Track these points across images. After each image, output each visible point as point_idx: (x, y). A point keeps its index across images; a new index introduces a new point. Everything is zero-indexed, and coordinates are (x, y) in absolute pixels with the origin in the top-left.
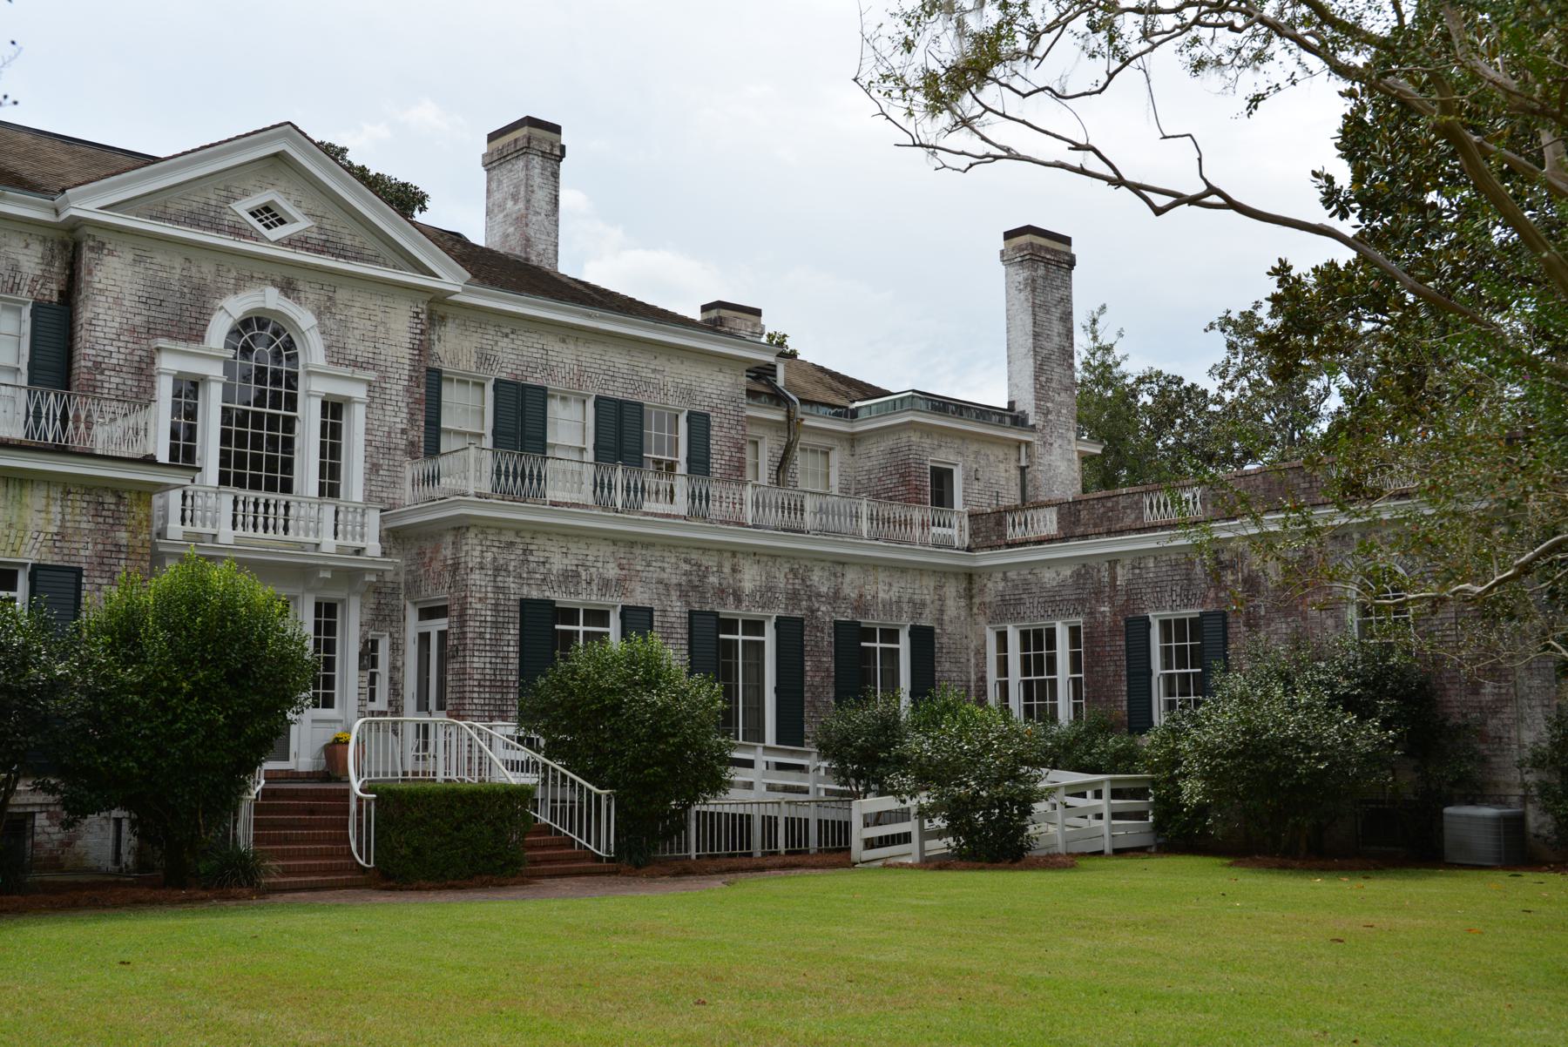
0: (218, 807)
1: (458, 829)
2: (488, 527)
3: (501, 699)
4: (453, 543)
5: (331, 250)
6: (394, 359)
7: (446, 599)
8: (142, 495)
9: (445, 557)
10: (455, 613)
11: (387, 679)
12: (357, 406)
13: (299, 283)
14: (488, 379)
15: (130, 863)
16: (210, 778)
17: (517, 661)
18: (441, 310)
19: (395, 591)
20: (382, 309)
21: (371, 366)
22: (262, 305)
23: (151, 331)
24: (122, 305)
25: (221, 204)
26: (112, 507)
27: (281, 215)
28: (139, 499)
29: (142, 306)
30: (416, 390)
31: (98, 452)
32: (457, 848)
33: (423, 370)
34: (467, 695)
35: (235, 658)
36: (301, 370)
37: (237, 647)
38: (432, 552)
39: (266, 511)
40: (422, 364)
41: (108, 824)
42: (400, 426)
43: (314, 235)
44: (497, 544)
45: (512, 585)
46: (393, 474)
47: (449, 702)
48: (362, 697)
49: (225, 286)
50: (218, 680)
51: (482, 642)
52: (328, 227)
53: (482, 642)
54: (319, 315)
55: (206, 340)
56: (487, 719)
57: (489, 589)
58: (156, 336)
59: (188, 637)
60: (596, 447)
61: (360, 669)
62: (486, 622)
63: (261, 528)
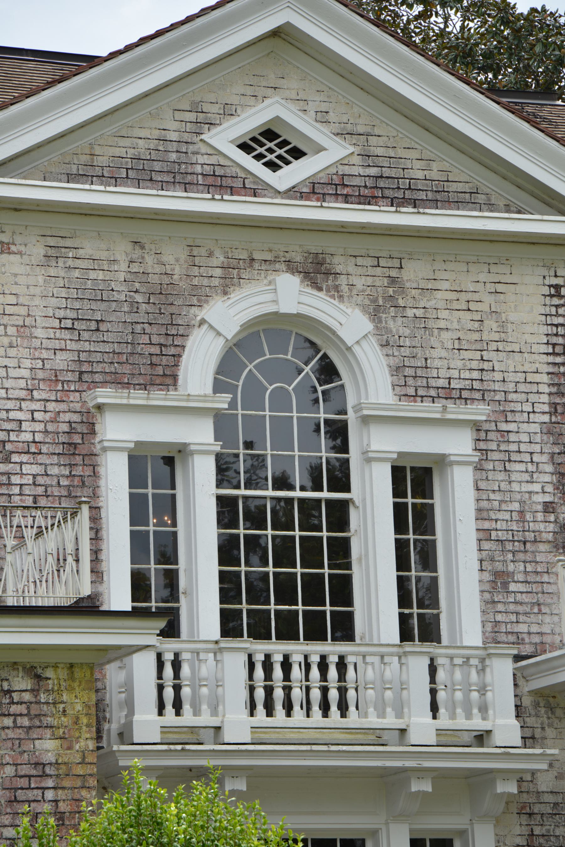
5: (387, 193)
6: (520, 377)
8: (76, 670)
13: (336, 260)
20: (491, 288)
21: (478, 395)
22: (272, 308)
23: (86, 377)
24: (32, 337)
25: (186, 137)
26: (27, 697)
27: (295, 142)
29: (66, 335)
31: (10, 602)
36: (351, 417)
39: (287, 677)
42: (540, 498)
43: (355, 171)
49: (205, 282)
52: (380, 151)
55: (180, 382)
58: (95, 384)
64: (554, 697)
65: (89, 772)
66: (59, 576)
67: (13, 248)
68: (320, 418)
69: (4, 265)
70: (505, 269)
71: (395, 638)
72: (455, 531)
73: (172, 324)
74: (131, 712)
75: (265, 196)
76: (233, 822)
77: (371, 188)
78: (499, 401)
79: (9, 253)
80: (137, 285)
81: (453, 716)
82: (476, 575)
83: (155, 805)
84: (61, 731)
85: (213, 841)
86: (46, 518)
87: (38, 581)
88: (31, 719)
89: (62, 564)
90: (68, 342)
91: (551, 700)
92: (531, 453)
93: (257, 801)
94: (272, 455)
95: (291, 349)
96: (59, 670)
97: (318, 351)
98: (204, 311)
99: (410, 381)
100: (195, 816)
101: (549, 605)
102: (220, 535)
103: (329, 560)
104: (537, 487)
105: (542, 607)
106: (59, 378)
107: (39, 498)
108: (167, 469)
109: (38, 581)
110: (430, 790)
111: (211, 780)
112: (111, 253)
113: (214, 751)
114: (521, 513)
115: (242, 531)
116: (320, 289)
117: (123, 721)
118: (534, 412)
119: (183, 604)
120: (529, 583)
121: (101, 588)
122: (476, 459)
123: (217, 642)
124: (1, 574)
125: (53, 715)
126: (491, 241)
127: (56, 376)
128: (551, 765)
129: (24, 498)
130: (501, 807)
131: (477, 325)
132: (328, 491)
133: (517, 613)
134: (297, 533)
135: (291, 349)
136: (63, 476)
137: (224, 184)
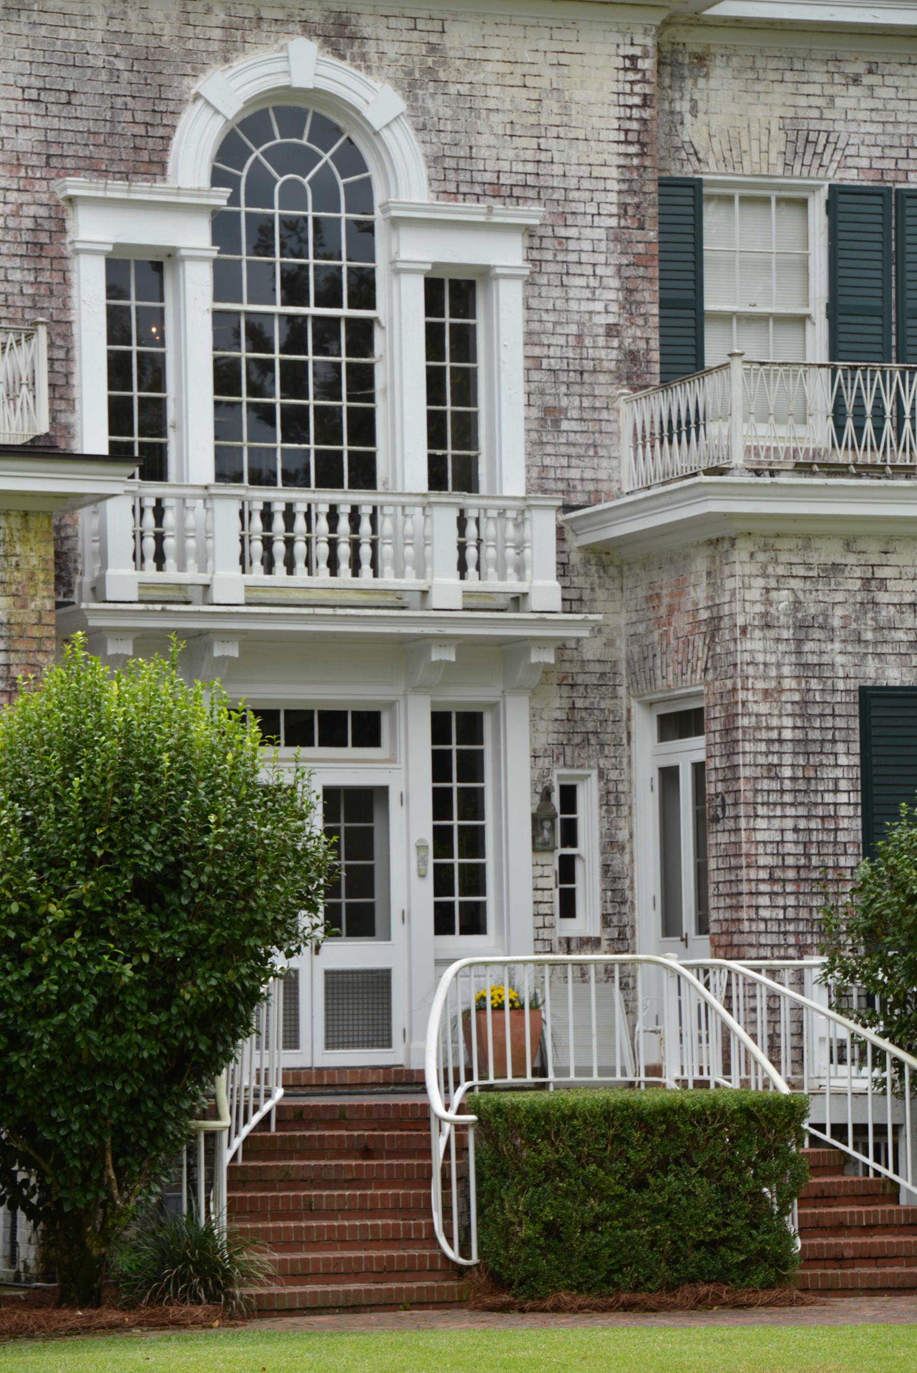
0: (144, 1143)
1: (641, 1185)
2: (778, 536)
4: (709, 574)
7: (699, 695)
9: (696, 604)
10: (716, 726)
13: (363, 21)
14: (815, 189)
15: (31, 1262)
16: (118, 1087)
17: (858, 823)
18: (695, 40)
20: (553, 58)
21: (532, 193)
22: (282, 81)
23: (54, 162)
28: (26, 527)
29: (30, 108)
30: (637, 235)
32: (638, 1224)
33: (651, 187)
34: (745, 900)
35: (150, 853)
36: (378, 217)
37: (154, 831)
38: (672, 595)
42: (603, 320)
44: (801, 571)
45: (840, 659)
46: (591, 426)
47: (714, 915)
48: (544, 909)
49: (202, 45)
50: (119, 895)
51: (775, 785)
55: (170, 170)
56: (792, 952)
57: (786, 670)
58: (65, 172)
60: (833, 311)
61: (535, 850)
62: (780, 741)
63: (280, 566)
64: (607, 553)
65: (46, 634)
70: (571, 35)
71: (423, 486)
72: (499, 359)
73: (160, 99)
74: (104, 566)
80: (118, 48)
84: (14, 587)
90: (33, 117)
91: (604, 557)
92: (594, 265)
96: (12, 519)
98: (200, 83)
101: (607, 447)
103: (348, 390)
104: (599, 306)
105: (599, 449)
108: (156, 275)
110: (453, 659)
113: (199, 612)
114: (579, 337)
116: (343, 57)
117: (97, 574)
118: (599, 214)
120: (585, 420)
122: (527, 272)
127: (18, 159)
131: (534, 105)
133: (569, 457)
136: (27, 282)
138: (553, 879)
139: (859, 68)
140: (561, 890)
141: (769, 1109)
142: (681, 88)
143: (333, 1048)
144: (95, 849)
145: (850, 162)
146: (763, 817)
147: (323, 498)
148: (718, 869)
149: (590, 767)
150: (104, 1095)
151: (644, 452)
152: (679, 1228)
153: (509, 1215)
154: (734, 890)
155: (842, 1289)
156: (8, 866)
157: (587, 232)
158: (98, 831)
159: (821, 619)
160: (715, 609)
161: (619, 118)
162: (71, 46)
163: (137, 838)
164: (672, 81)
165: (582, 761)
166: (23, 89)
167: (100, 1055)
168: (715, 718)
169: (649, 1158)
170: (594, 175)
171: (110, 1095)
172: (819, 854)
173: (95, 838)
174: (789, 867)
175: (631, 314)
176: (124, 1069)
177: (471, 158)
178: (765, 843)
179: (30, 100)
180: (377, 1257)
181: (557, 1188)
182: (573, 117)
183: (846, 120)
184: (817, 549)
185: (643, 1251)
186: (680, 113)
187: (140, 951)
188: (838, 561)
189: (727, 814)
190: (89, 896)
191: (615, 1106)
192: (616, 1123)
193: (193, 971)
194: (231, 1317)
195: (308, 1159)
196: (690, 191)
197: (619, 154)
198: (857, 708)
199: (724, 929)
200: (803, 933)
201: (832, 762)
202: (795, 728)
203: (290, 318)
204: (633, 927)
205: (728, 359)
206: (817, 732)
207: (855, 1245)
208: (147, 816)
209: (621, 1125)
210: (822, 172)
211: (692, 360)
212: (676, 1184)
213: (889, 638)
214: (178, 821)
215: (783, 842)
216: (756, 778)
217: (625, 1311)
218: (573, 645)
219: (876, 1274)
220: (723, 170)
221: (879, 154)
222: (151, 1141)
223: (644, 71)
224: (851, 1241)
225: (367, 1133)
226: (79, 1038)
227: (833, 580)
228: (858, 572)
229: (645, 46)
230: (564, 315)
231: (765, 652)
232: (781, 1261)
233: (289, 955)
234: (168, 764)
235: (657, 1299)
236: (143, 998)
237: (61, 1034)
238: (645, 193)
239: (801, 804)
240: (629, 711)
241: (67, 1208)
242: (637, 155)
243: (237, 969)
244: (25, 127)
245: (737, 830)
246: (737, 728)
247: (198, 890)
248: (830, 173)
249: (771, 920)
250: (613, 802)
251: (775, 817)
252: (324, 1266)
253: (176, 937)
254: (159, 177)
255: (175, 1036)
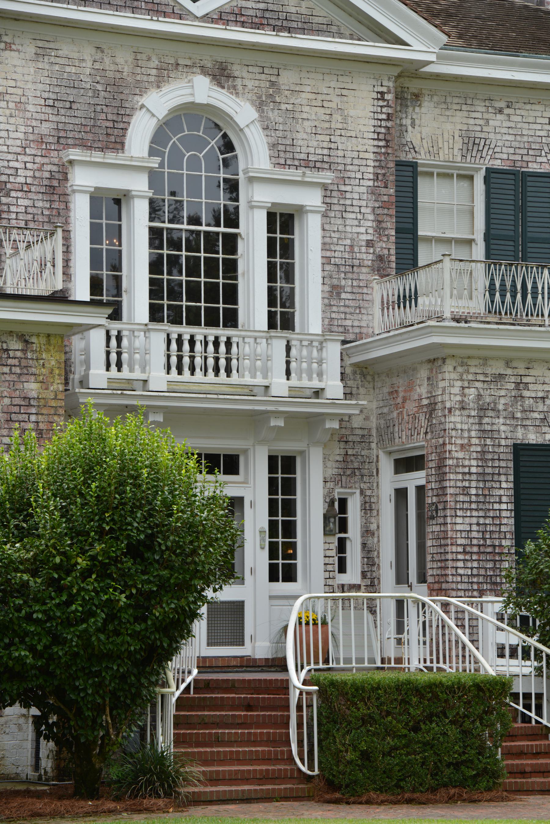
0: (128, 701)
1: (416, 729)
2: (469, 358)
3: (494, 569)
4: (429, 379)
5: (271, 22)
6: (355, 154)
7: (422, 447)
8: (52, 338)
9: (420, 395)
10: (432, 464)
11: (359, 547)
12: (310, 216)
13: (235, 67)
14: (478, 170)
15: (49, 769)
16: (115, 668)
17: (512, 521)
18: (414, 86)
19: (365, 440)
20: (338, 92)
21: (326, 166)
22: (190, 99)
23: (62, 141)
24: (26, 110)
26: (19, 354)
29: (49, 110)
30: (384, 191)
31: (9, 291)
32: (415, 753)
33: (392, 165)
34: (450, 564)
35: (137, 528)
36: (241, 177)
37: (139, 515)
38: (405, 391)
39: (192, 350)
40: (390, 158)
41: (27, 723)
42: (364, 237)
44: (481, 378)
45: (503, 428)
46: (358, 297)
47: (430, 572)
48: (330, 568)
49: (145, 78)
50: (119, 553)
51: (467, 499)
53: (467, 499)
54: (260, 106)
55: (126, 147)
56: (475, 593)
57: (473, 434)
59: (83, 505)
60: (488, 237)
61: (325, 534)
62: (470, 473)
64: (366, 368)
65: (59, 405)
66: (41, 276)
67: (13, 47)
68: (220, 177)
69: (7, 59)
70: (349, 79)
71: (265, 327)
72: (307, 257)
73: (122, 107)
74: (88, 368)
75: (187, 19)
76: (152, 441)
77: (260, 17)
78: (340, 170)
79: (11, 50)
80: (98, 78)
81: (300, 379)
82: (320, 287)
83: (101, 428)
84: (41, 378)
85: (139, 452)
86: (33, 236)
87: (27, 279)
88: (21, 369)
89: (43, 267)
90: (50, 115)
91: (364, 370)
92: (360, 207)
93: (169, 428)
94: (187, 201)
95: (202, 128)
96: (40, 338)
97: (221, 130)
98: (144, 99)
99: (282, 154)
100: (128, 436)
101: (366, 308)
102: (150, 254)
103: (223, 273)
104: (362, 230)
105: (362, 310)
106: (44, 140)
107: (29, 222)
108: (116, 207)
109: (27, 279)
110: (283, 425)
111: (139, 413)
112: (81, 54)
113: (142, 395)
114: (352, 246)
115: (165, 252)
116: (223, 87)
117: (83, 373)
118: (363, 179)
119: (125, 299)
120: (354, 293)
121: (70, 285)
122: (324, 209)
123: (146, 325)
124: (2, 272)
125: (36, 367)
126: (340, 59)
127: (42, 139)
128: (361, 411)
129: (19, 221)
130: (329, 436)
131: (328, 117)
132: (224, 227)
133: (346, 313)
134: (202, 255)
135: (202, 128)
136: (45, 208)
137: (160, 10)
138: (335, 551)
139: (502, 104)
140: (339, 557)
141: (490, 685)
142: (406, 112)
143: (212, 646)
144: (104, 525)
145: (497, 156)
146: (460, 517)
147: (212, 332)
148: (433, 546)
149: (355, 488)
150: (107, 672)
151: (388, 312)
152: (438, 755)
153: (339, 746)
154: (443, 558)
155: (526, 791)
156: (54, 535)
157: (356, 189)
158: (107, 515)
159: (492, 405)
160: (432, 399)
161: (374, 126)
162: (72, 76)
163: (129, 519)
164: (401, 107)
165: (351, 485)
166: (45, 99)
167: (105, 648)
168: (432, 460)
169: (422, 713)
170: (360, 157)
171: (110, 673)
172: (491, 538)
173: (104, 519)
174: (474, 545)
175: (380, 235)
176: (119, 657)
177: (293, 145)
178: (461, 531)
179: (49, 106)
180: (260, 770)
181: (368, 731)
182: (349, 125)
183: (495, 133)
184: (490, 366)
185: (417, 768)
186: (406, 125)
187: (132, 586)
188: (502, 373)
189: (439, 515)
190: (102, 553)
191: (402, 682)
192: (403, 692)
193: (160, 599)
194: (179, 806)
195: (214, 711)
196: (411, 169)
197: (375, 146)
198: (512, 456)
199: (437, 580)
200: (482, 583)
201: (498, 486)
202: (478, 466)
203: (192, 232)
204: (379, 579)
205: (442, 258)
206: (490, 469)
207: (532, 765)
208: (134, 506)
209: (406, 694)
210: (482, 161)
211: (411, 262)
212: (437, 729)
213: (529, 417)
214: (153, 509)
215: (471, 531)
216: (457, 494)
217: (407, 803)
218: (347, 419)
219: (545, 782)
220: (428, 158)
221: (513, 152)
222: (133, 700)
223: (388, 101)
224: (529, 762)
225: (249, 696)
226: (94, 639)
227: (499, 383)
228: (513, 379)
229: (388, 87)
230: (343, 234)
231: (462, 423)
232: (495, 775)
233: (215, 590)
234: (146, 475)
235: (426, 797)
236: (131, 615)
237: (84, 636)
238: (388, 168)
239: (481, 509)
240: (377, 457)
241: (82, 740)
242: (384, 147)
243: (186, 598)
244: (46, 121)
245: (445, 524)
246: (446, 466)
247: (165, 551)
248: (487, 162)
249: (464, 575)
250: (368, 508)
251: (466, 516)
252: (229, 775)
253: (152, 579)
254: (120, 151)
255: (149, 638)
